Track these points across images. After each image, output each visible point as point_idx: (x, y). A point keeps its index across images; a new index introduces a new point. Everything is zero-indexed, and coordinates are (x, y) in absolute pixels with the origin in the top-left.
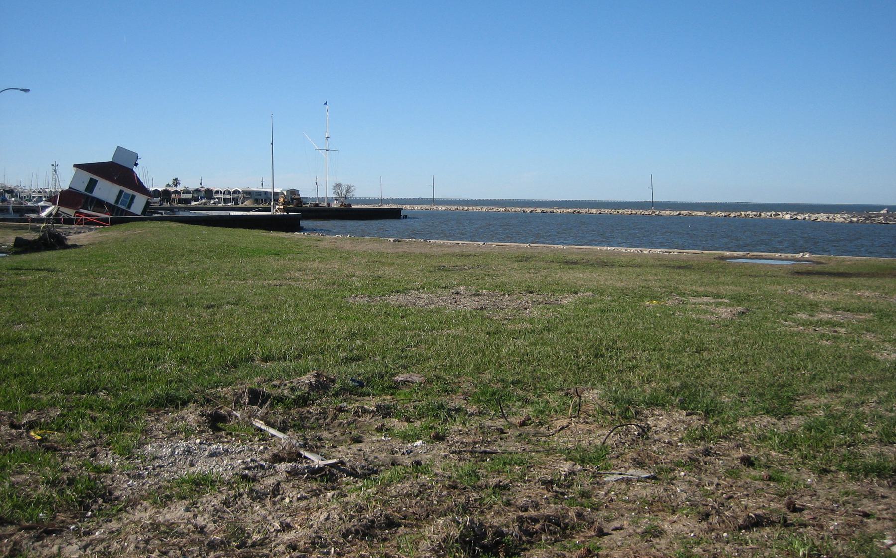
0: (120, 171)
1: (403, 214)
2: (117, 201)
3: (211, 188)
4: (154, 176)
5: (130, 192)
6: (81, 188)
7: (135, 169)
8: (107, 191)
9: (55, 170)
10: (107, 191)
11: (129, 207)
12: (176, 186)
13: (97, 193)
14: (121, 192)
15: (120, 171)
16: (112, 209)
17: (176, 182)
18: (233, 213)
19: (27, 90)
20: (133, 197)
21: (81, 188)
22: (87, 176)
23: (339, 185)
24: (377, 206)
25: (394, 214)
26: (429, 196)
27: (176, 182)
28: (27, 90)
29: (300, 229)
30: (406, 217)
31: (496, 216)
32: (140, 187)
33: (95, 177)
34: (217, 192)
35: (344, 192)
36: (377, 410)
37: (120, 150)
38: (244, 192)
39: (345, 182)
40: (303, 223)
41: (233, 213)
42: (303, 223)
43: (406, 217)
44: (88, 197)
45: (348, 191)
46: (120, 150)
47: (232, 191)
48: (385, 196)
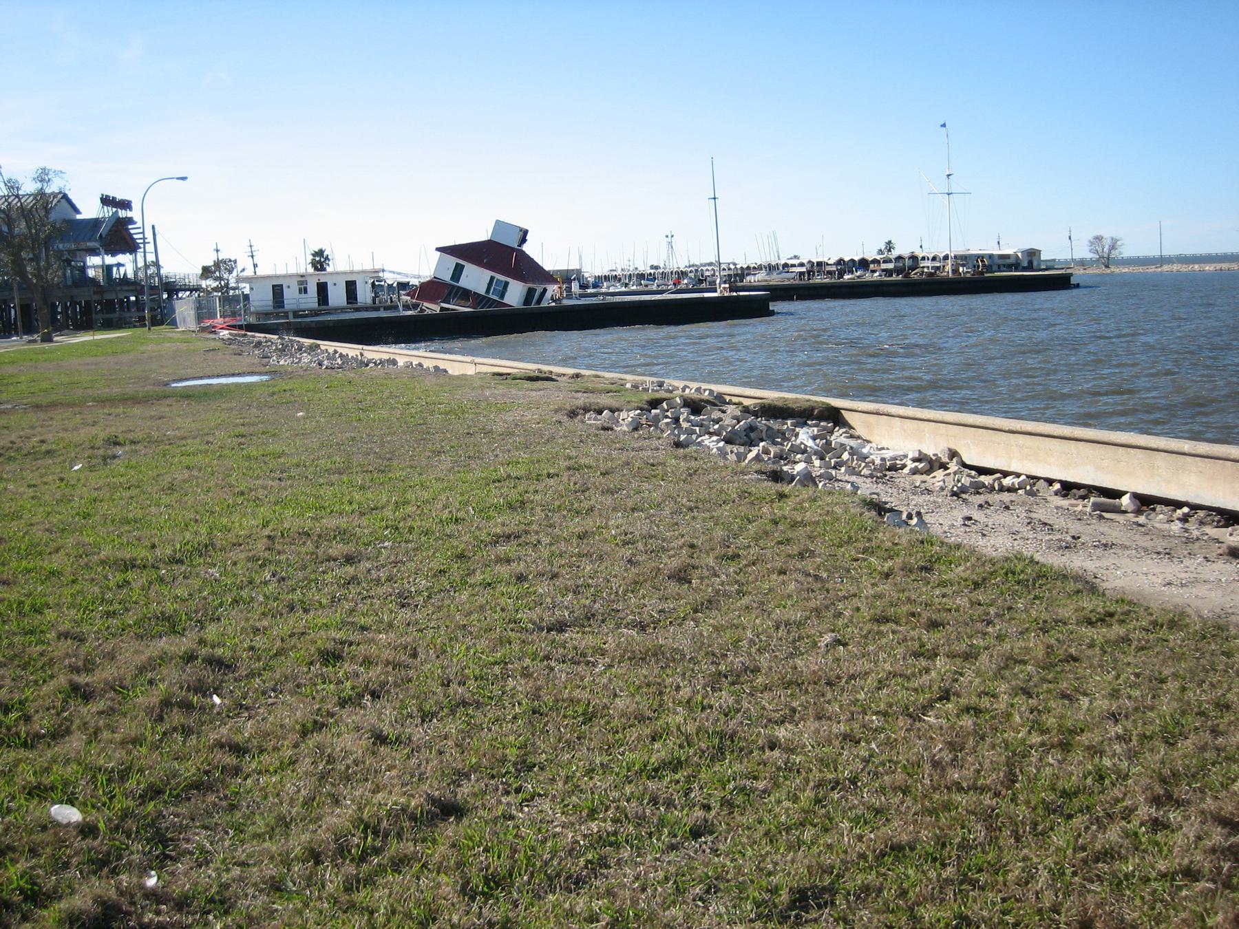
0: (503, 254)
1: (1073, 281)
2: (488, 291)
4: (546, 252)
6: (447, 277)
7: (526, 248)
8: (476, 278)
9: (670, 243)
10: (476, 278)
11: (502, 296)
13: (464, 282)
14: (492, 278)
17: (889, 246)
18: (707, 295)
19: (184, 179)
20: (507, 284)
21: (447, 277)
22: (452, 261)
23: (1099, 239)
25: (1060, 282)
26: (1153, 252)
27: (889, 246)
28: (184, 179)
29: (772, 313)
30: (1078, 286)
31: (1206, 278)
34: (923, 258)
37: (499, 224)
39: (1107, 234)
40: (773, 306)
41: (707, 295)
42: (773, 306)
43: (1078, 286)
44: (454, 286)
45: (1113, 247)
46: (499, 224)
48: (1166, 253)
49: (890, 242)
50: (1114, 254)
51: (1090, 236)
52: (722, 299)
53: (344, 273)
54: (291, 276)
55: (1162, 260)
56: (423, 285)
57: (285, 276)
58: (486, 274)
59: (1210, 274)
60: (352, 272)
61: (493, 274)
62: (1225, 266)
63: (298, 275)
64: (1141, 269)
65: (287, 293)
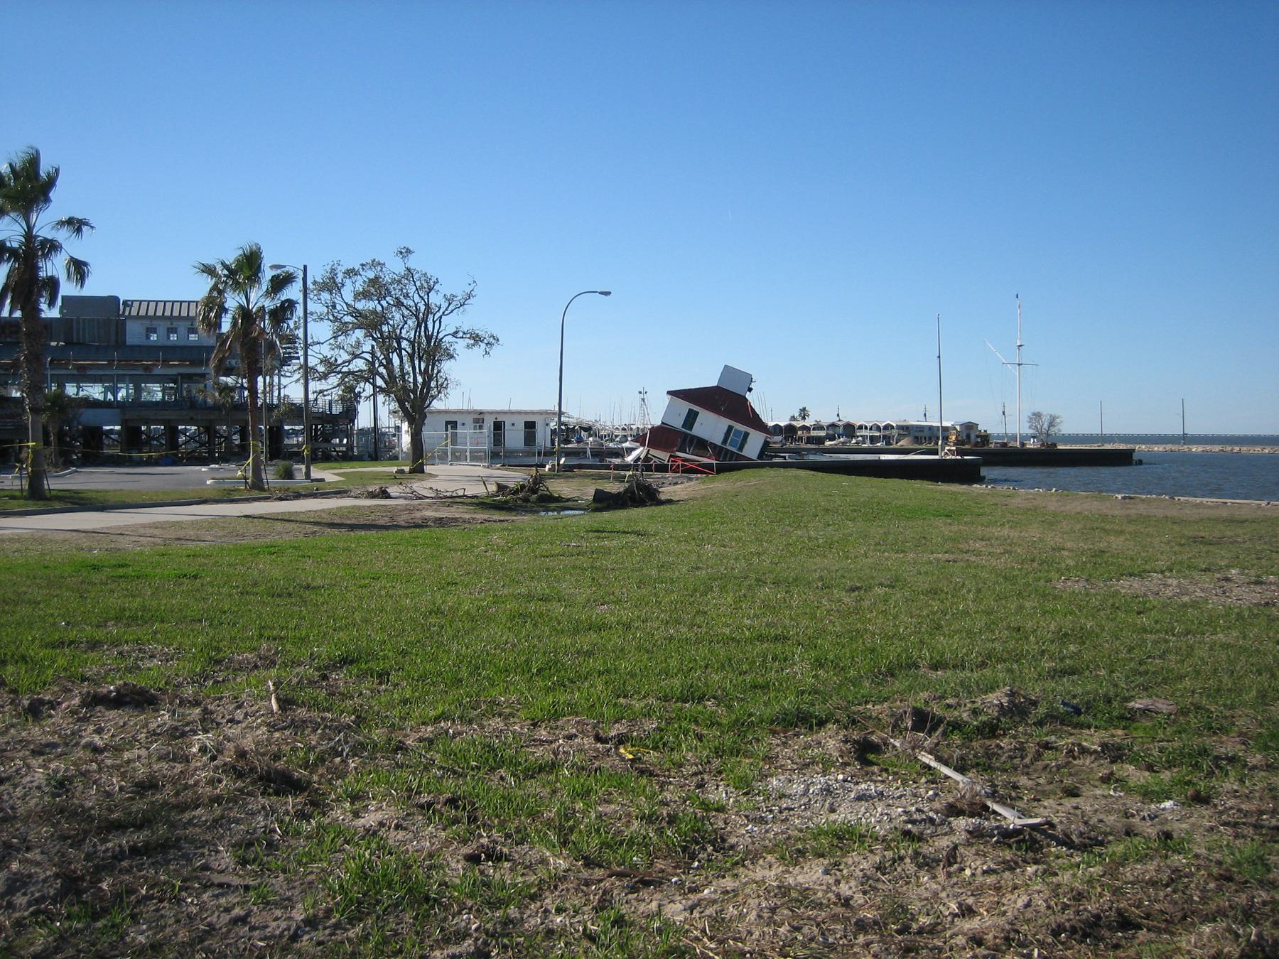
0: (727, 399)
1: (1135, 457)
2: (725, 441)
3: (852, 421)
5: (742, 428)
6: (678, 423)
8: (711, 426)
10: (711, 426)
11: (741, 448)
12: (804, 418)
13: (698, 430)
14: (730, 428)
15: (727, 399)
16: (718, 451)
17: (804, 414)
19: (607, 294)
20: (747, 435)
21: (678, 423)
22: (684, 407)
23: (1038, 415)
24: (1095, 447)
25: (1121, 458)
26: (1096, 431)
27: (804, 414)
28: (607, 294)
29: (980, 480)
30: (1140, 462)
31: (1252, 460)
32: (754, 421)
33: (696, 408)
34: (861, 427)
35: (1046, 426)
36: (1103, 751)
38: (900, 427)
39: (1047, 410)
40: (984, 471)
42: (984, 471)
43: (1140, 462)
44: (687, 435)
45: (1051, 424)
47: (882, 425)
49: (804, 409)
50: (1053, 431)
51: (1027, 413)
52: (942, 462)
53: (526, 413)
54: (468, 412)
55: (1185, 439)
56: (653, 430)
57: (505, 413)
58: (724, 423)
59: (1196, 455)
60: (533, 413)
61: (729, 422)
62: (1175, 447)
63: (475, 412)
64: (1175, 447)
65: (539, 428)
